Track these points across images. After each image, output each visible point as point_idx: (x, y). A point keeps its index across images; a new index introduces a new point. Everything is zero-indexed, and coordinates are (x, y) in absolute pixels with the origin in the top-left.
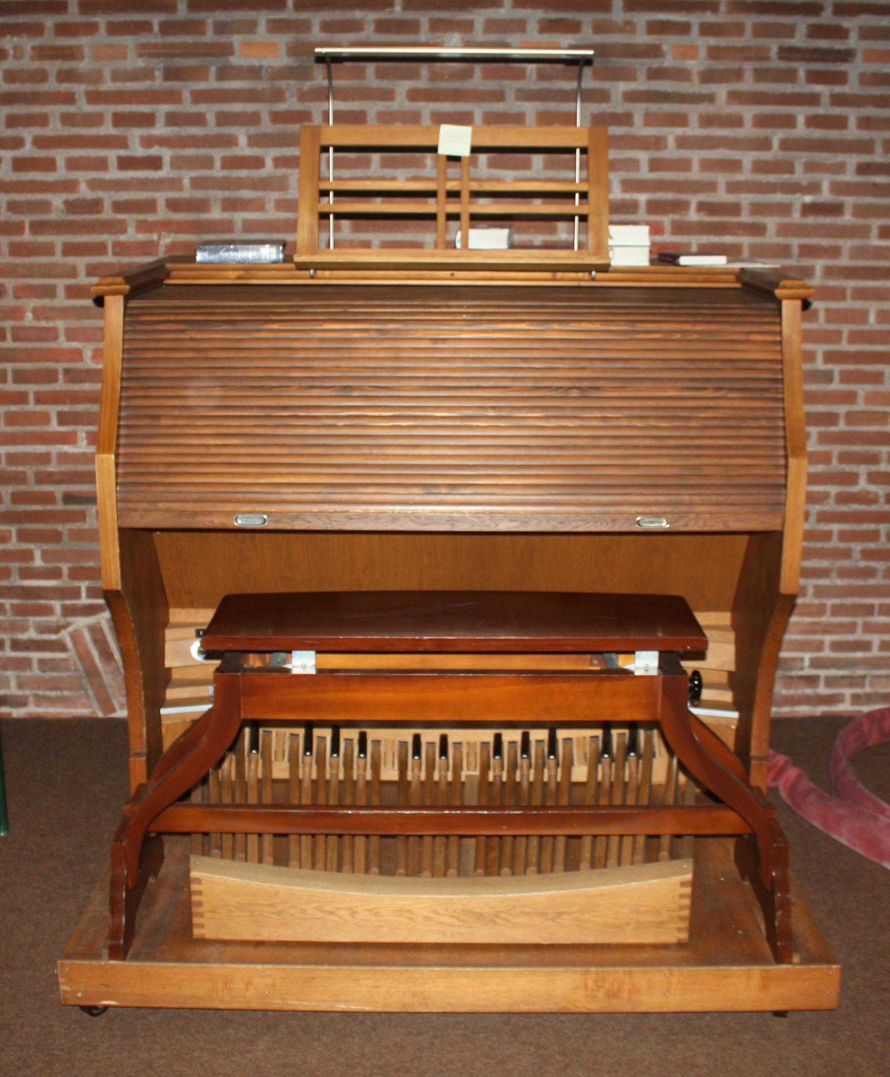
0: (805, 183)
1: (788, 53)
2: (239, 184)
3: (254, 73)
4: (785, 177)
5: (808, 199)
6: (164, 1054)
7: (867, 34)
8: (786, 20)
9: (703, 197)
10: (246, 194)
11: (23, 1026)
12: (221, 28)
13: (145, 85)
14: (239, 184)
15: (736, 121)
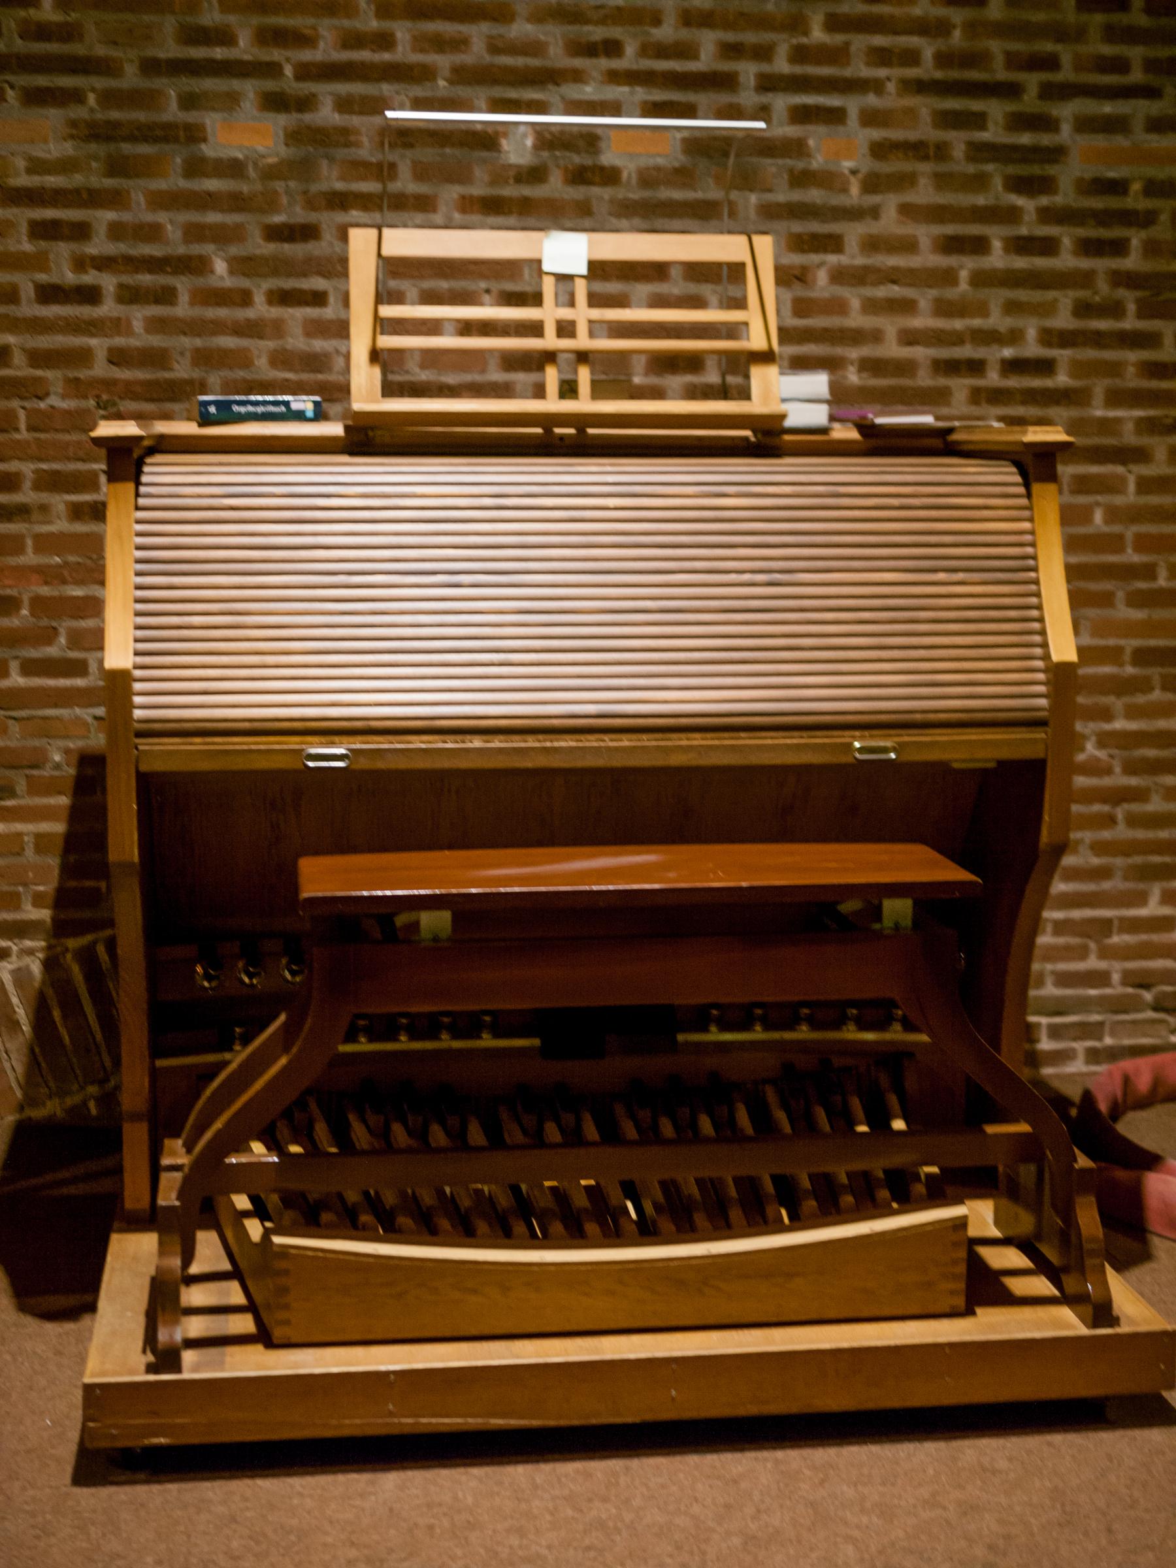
0: (1002, 329)
1: (979, 151)
2: (219, 327)
3: (234, 168)
4: (977, 322)
5: (1008, 353)
6: (248, 1504)
7: (1085, 125)
8: (976, 105)
9: (866, 351)
10: (228, 342)
11: (24, 1489)
12: (189, 101)
13: (79, 179)
14: (219, 327)
15: (909, 246)
